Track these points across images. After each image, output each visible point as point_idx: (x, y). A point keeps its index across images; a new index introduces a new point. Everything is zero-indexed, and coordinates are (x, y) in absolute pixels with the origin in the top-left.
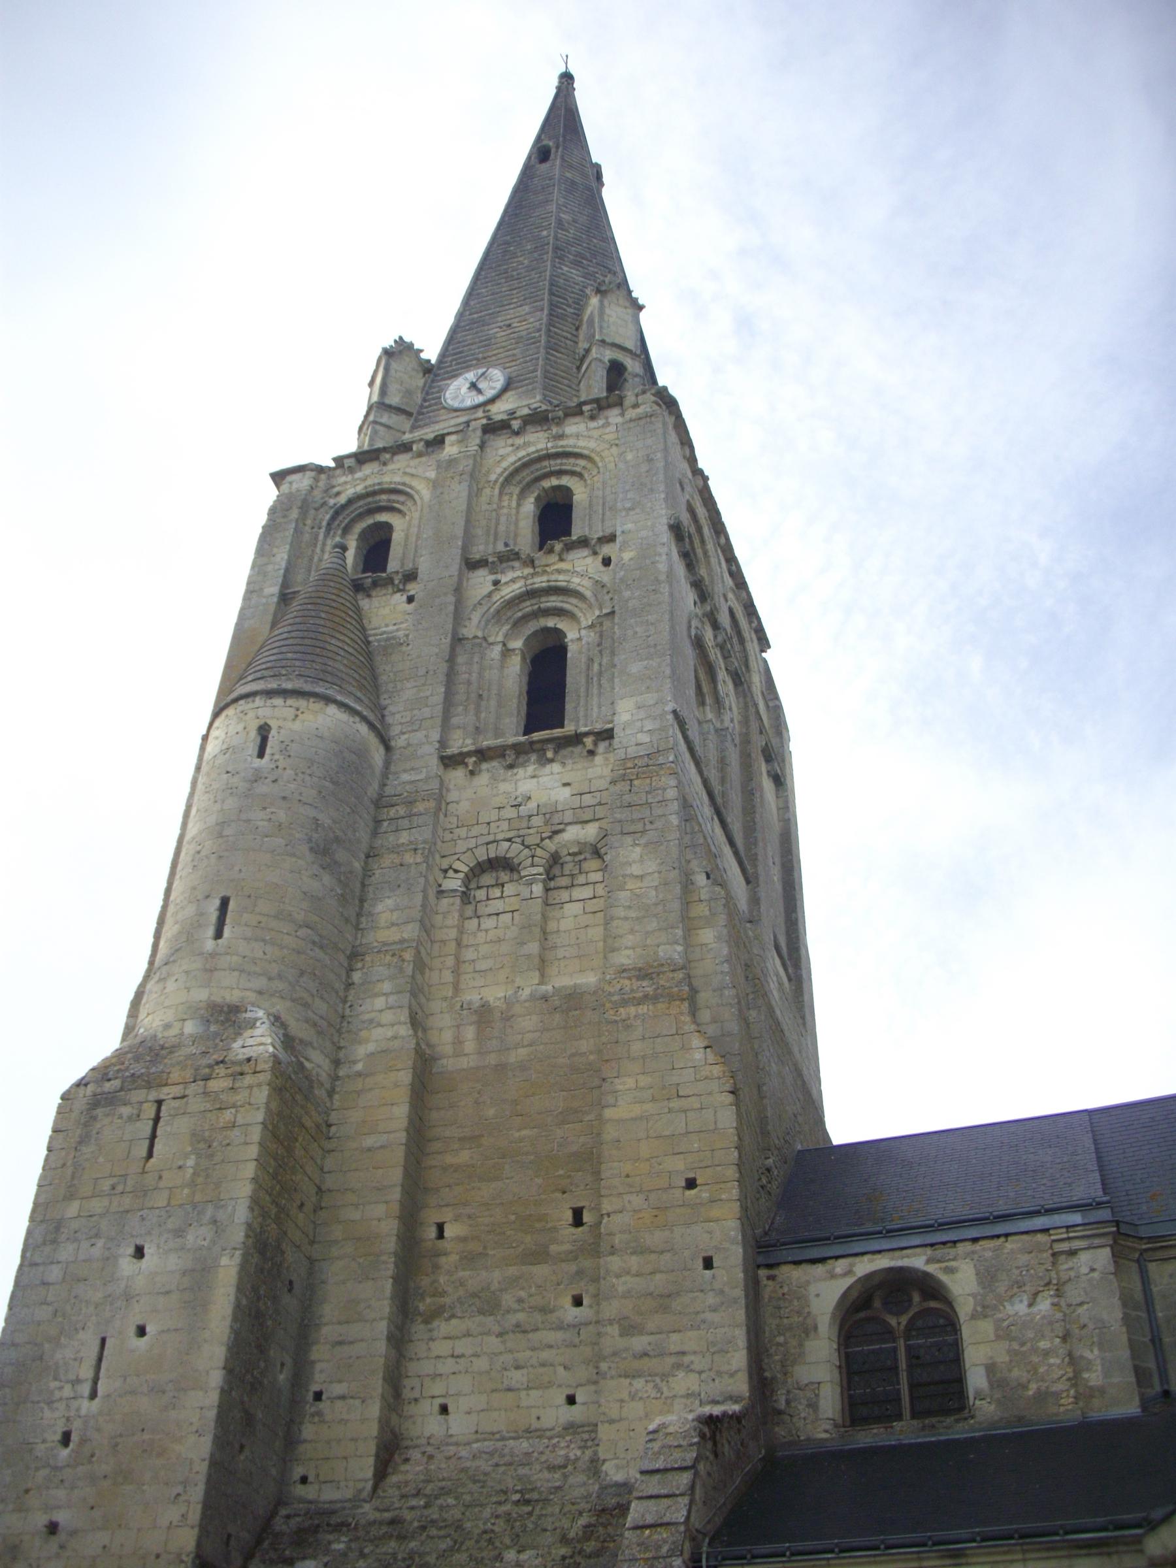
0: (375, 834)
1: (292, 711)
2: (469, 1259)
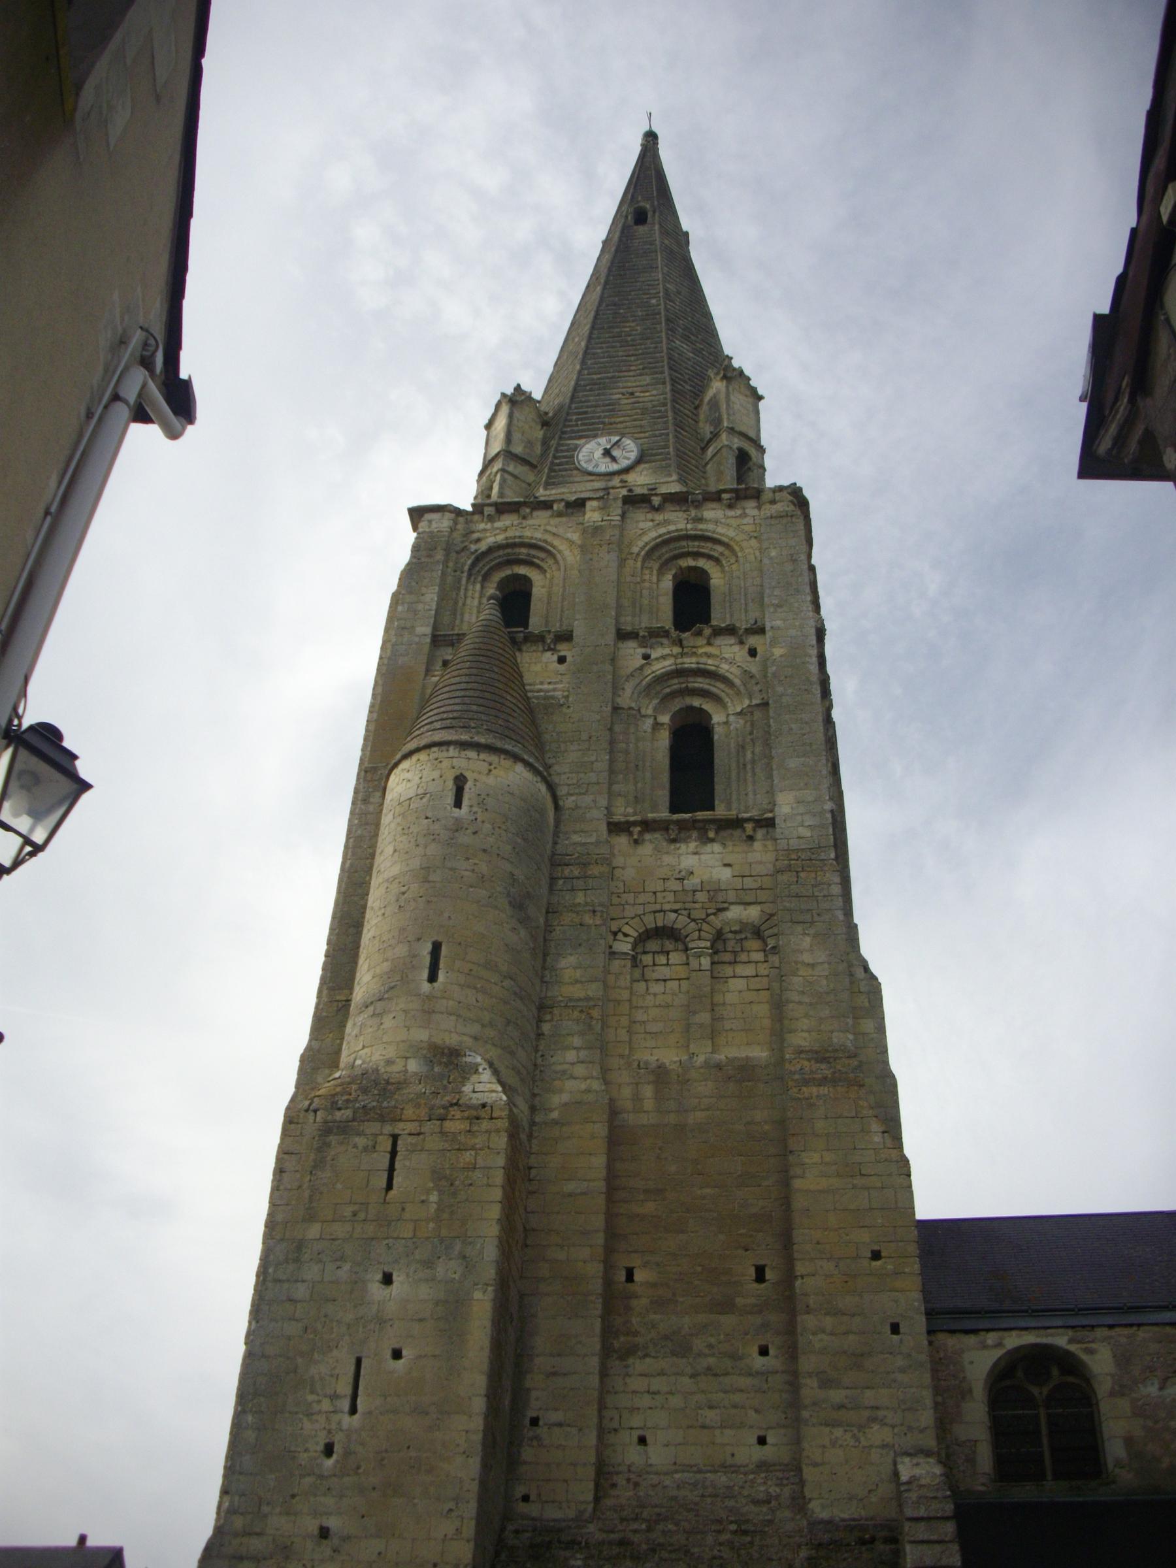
0: (551, 890)
1: (486, 764)
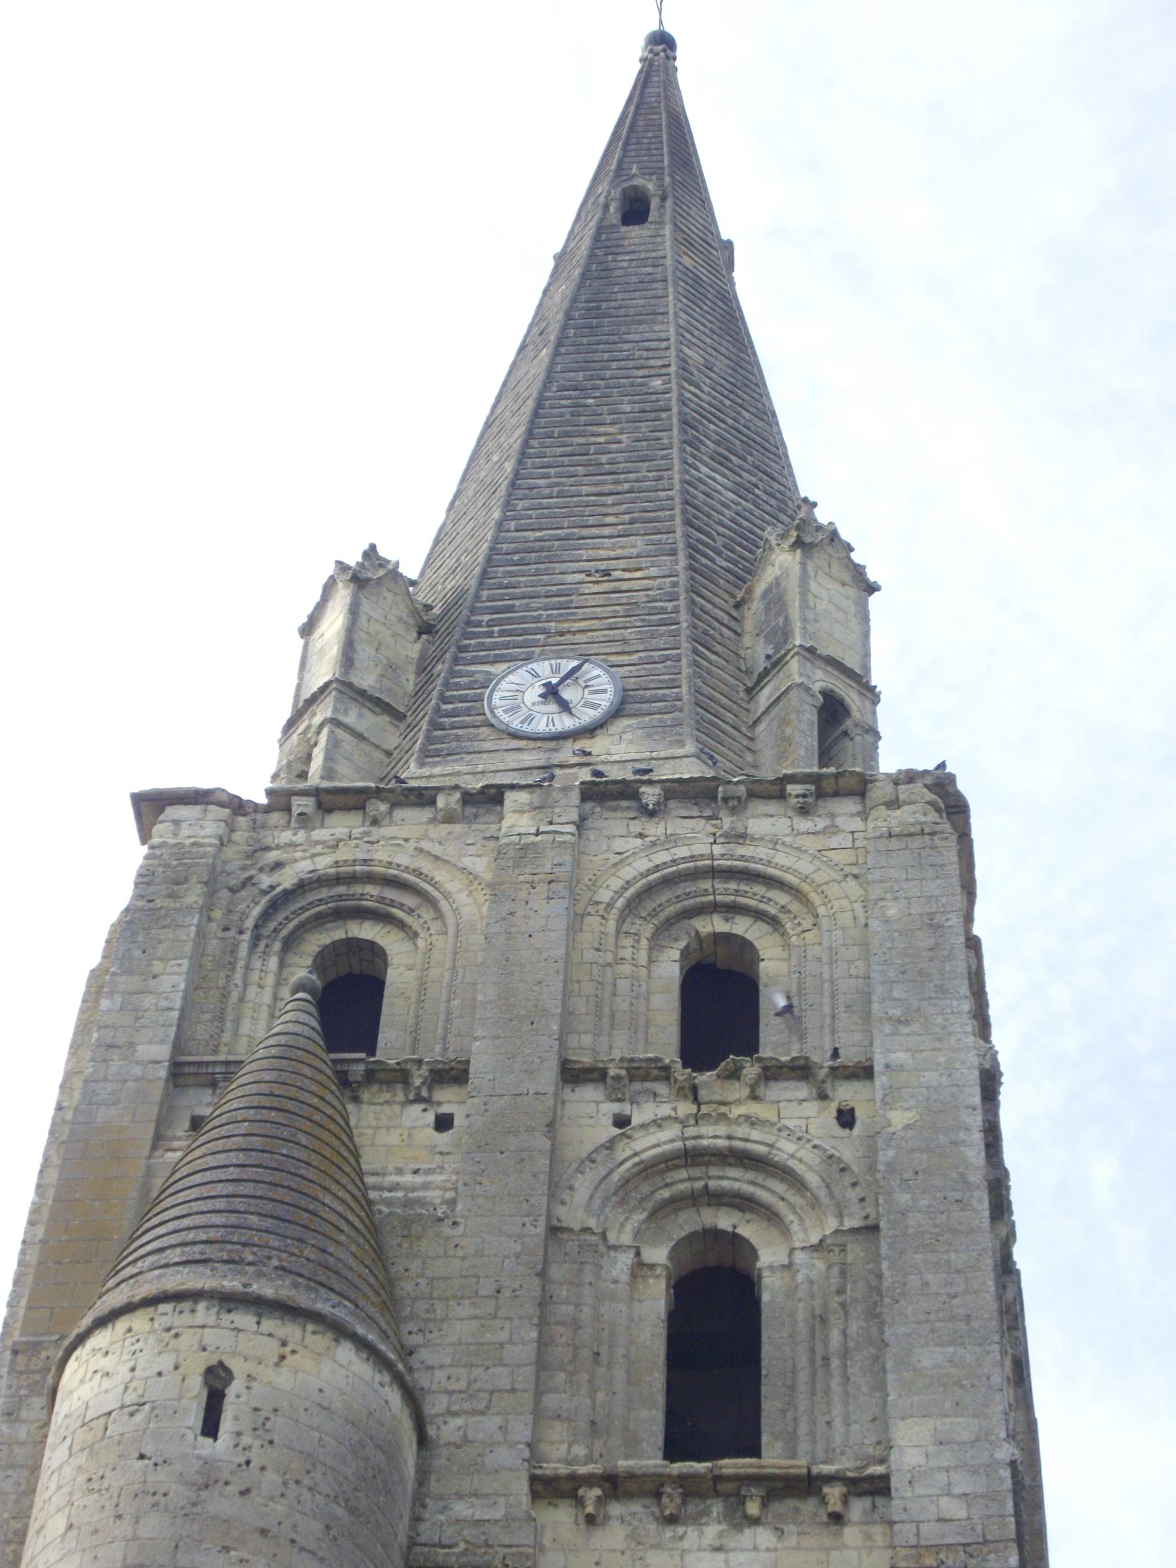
1: (274, 1344)
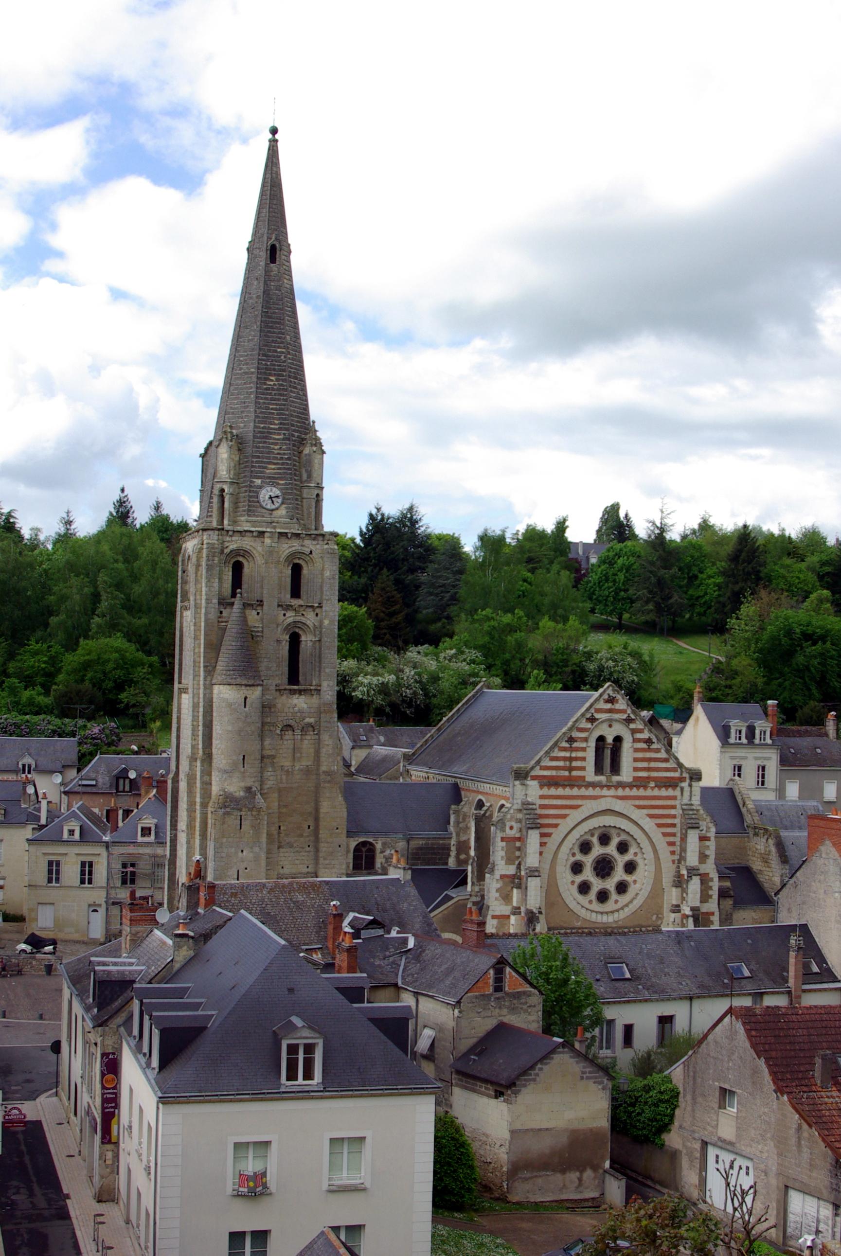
2: (287, 835)
